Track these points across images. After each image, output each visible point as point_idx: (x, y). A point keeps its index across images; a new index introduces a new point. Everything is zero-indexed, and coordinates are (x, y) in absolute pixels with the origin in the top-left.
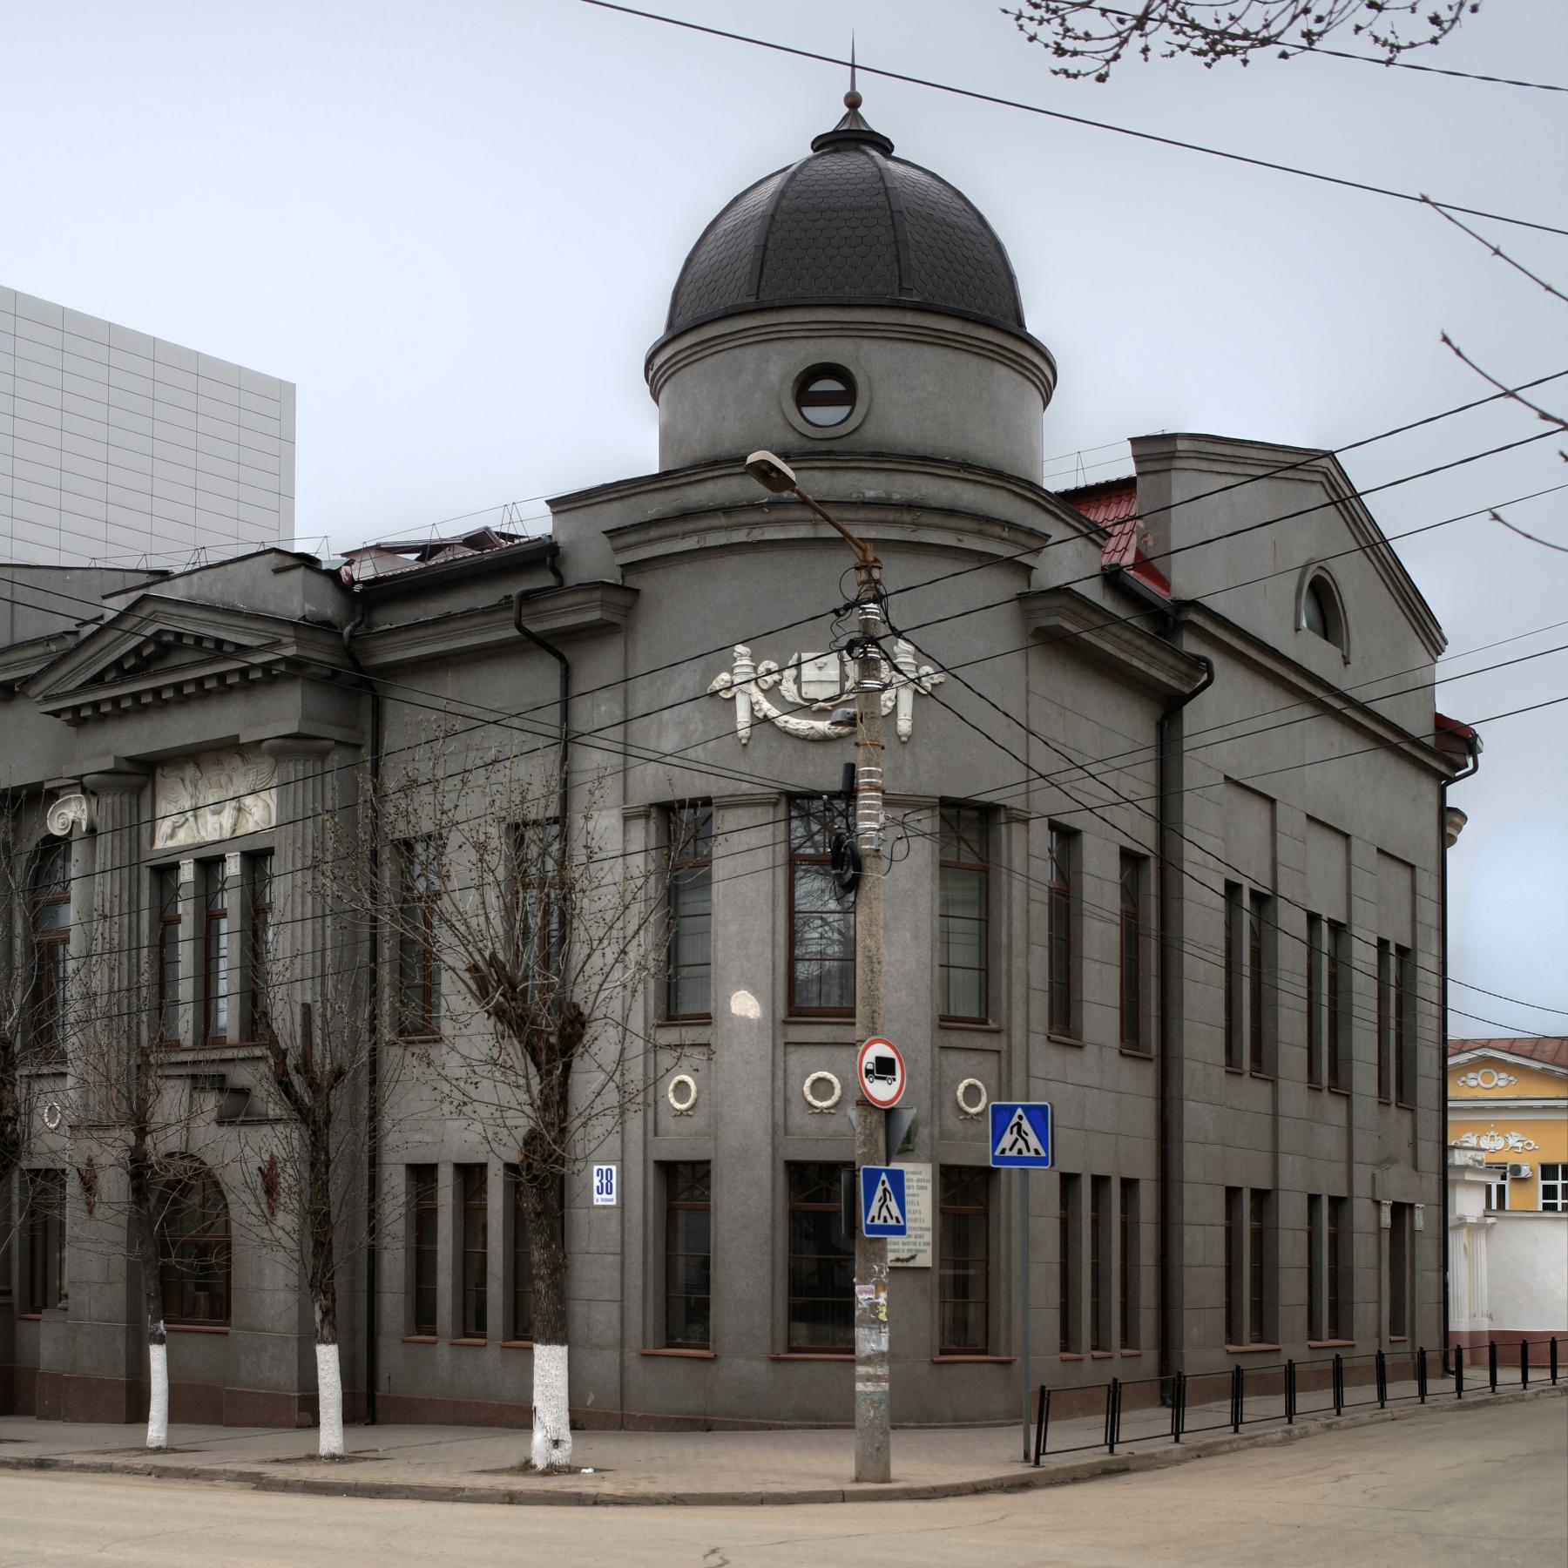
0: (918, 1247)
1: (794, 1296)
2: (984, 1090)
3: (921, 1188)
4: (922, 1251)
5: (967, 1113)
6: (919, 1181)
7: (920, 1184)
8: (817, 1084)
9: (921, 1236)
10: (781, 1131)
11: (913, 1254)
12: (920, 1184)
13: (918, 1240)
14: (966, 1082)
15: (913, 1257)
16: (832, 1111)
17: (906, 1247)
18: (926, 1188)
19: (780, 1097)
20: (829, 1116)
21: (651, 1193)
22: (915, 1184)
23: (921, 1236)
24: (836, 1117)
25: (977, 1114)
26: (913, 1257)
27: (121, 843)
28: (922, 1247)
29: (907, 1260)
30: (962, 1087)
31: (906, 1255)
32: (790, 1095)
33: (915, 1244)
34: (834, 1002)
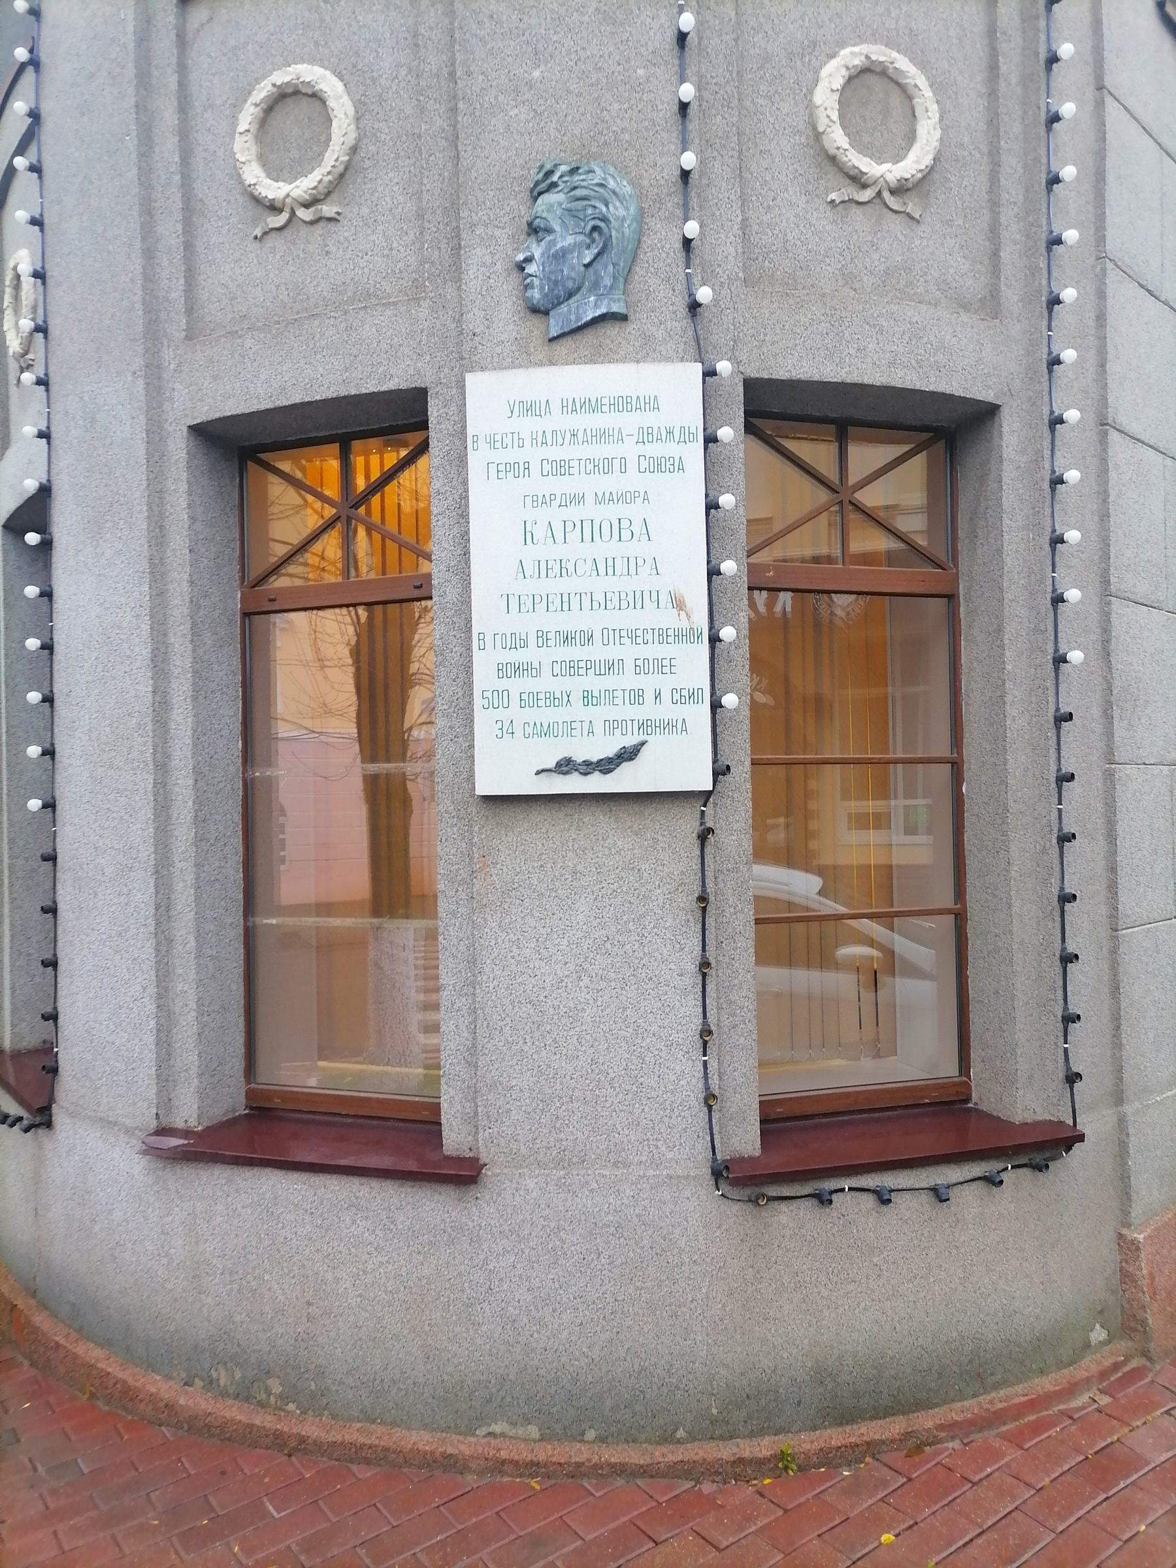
0: (648, 711)
1: (373, 759)
2: (922, 81)
3: (659, 466)
4: (668, 726)
5: (858, 180)
6: (646, 436)
7: (655, 450)
8: (277, 118)
9: (661, 667)
10: (177, 325)
11: (630, 741)
12: (655, 450)
13: (648, 683)
14: (852, 55)
15: (628, 755)
16: (328, 210)
17: (599, 714)
18: (681, 727)
19: (170, 200)
20: (319, 229)
21: (179, 541)
22: (630, 450)
23: (661, 667)
24: (342, 231)
25: (901, 189)
26: (628, 755)
27: (836, 533)
28: (667, 711)
29: (607, 766)
30: (833, 74)
31: (605, 747)
32: (200, 188)
33: (637, 697)
34: (756, 592)
